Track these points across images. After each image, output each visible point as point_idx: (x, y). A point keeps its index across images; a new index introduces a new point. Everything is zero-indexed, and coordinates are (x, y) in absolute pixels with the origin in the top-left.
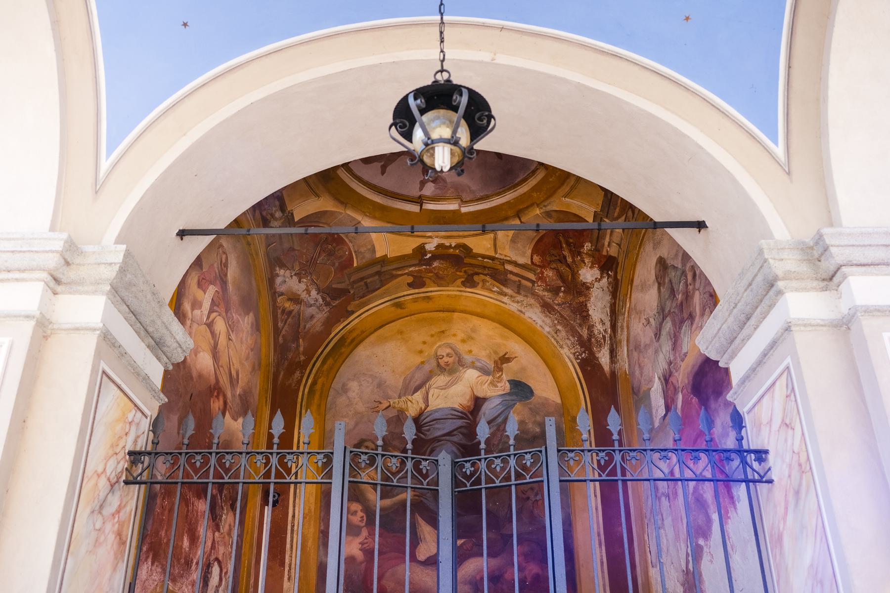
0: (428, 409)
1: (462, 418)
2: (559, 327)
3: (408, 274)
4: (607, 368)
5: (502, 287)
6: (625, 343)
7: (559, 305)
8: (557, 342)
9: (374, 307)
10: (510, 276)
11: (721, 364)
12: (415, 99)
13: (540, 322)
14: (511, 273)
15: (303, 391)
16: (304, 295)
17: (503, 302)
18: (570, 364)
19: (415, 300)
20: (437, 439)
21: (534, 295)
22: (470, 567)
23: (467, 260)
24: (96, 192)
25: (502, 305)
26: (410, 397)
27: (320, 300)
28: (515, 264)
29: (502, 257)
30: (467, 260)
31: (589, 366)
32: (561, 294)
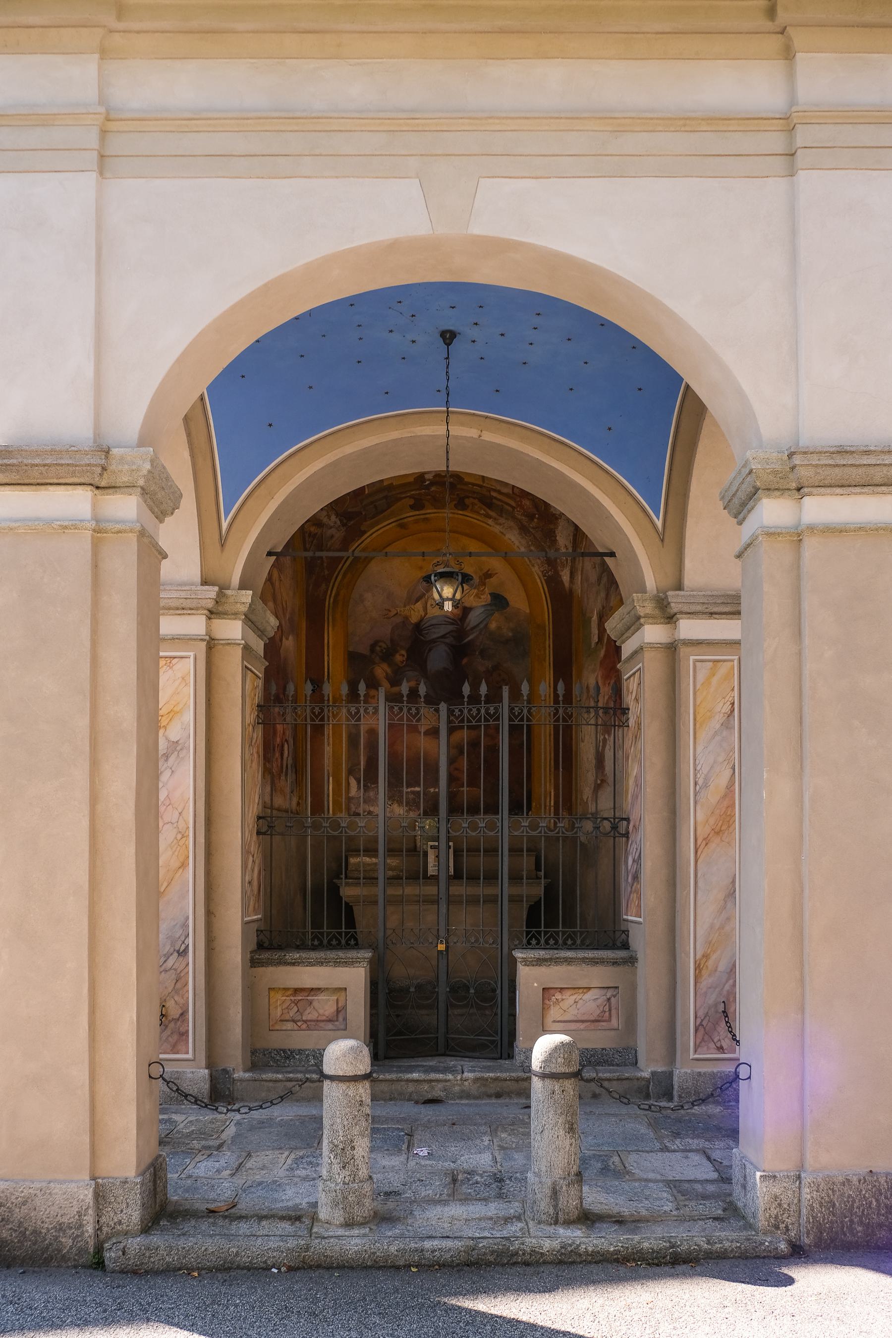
0: (427, 616)
1: (452, 624)
2: (532, 548)
3: (410, 497)
4: (567, 584)
5: (488, 510)
6: (579, 573)
7: (533, 528)
8: (530, 561)
9: (380, 528)
10: (494, 501)
11: (617, 644)
12: (435, 576)
13: (517, 543)
14: (495, 498)
15: (329, 602)
16: (325, 520)
17: (488, 524)
18: (538, 580)
19: (416, 522)
20: (434, 641)
21: (514, 518)
22: (457, 736)
23: (459, 486)
24: (222, 546)
25: (488, 527)
26: (412, 607)
27: (339, 522)
28: (499, 492)
29: (488, 486)
30: (459, 486)
31: (553, 582)
32: (536, 520)
